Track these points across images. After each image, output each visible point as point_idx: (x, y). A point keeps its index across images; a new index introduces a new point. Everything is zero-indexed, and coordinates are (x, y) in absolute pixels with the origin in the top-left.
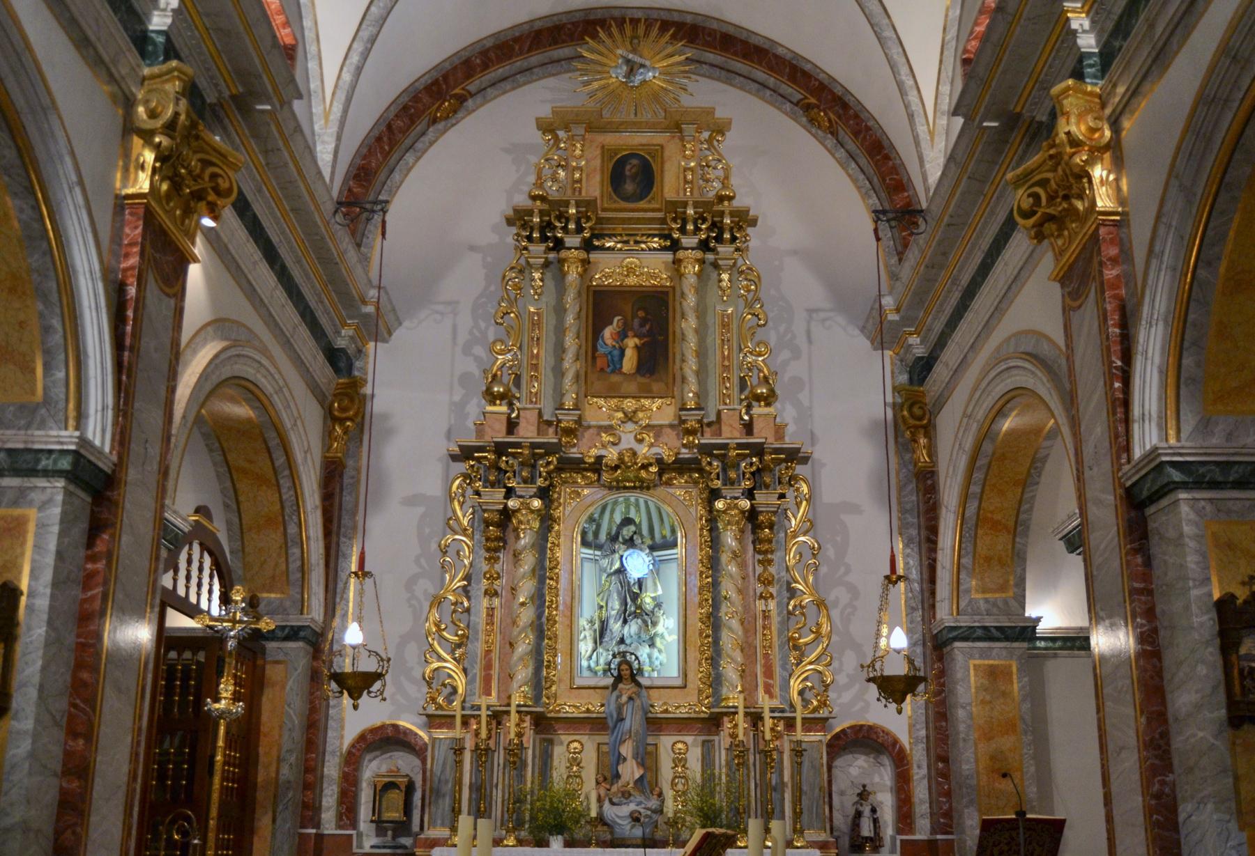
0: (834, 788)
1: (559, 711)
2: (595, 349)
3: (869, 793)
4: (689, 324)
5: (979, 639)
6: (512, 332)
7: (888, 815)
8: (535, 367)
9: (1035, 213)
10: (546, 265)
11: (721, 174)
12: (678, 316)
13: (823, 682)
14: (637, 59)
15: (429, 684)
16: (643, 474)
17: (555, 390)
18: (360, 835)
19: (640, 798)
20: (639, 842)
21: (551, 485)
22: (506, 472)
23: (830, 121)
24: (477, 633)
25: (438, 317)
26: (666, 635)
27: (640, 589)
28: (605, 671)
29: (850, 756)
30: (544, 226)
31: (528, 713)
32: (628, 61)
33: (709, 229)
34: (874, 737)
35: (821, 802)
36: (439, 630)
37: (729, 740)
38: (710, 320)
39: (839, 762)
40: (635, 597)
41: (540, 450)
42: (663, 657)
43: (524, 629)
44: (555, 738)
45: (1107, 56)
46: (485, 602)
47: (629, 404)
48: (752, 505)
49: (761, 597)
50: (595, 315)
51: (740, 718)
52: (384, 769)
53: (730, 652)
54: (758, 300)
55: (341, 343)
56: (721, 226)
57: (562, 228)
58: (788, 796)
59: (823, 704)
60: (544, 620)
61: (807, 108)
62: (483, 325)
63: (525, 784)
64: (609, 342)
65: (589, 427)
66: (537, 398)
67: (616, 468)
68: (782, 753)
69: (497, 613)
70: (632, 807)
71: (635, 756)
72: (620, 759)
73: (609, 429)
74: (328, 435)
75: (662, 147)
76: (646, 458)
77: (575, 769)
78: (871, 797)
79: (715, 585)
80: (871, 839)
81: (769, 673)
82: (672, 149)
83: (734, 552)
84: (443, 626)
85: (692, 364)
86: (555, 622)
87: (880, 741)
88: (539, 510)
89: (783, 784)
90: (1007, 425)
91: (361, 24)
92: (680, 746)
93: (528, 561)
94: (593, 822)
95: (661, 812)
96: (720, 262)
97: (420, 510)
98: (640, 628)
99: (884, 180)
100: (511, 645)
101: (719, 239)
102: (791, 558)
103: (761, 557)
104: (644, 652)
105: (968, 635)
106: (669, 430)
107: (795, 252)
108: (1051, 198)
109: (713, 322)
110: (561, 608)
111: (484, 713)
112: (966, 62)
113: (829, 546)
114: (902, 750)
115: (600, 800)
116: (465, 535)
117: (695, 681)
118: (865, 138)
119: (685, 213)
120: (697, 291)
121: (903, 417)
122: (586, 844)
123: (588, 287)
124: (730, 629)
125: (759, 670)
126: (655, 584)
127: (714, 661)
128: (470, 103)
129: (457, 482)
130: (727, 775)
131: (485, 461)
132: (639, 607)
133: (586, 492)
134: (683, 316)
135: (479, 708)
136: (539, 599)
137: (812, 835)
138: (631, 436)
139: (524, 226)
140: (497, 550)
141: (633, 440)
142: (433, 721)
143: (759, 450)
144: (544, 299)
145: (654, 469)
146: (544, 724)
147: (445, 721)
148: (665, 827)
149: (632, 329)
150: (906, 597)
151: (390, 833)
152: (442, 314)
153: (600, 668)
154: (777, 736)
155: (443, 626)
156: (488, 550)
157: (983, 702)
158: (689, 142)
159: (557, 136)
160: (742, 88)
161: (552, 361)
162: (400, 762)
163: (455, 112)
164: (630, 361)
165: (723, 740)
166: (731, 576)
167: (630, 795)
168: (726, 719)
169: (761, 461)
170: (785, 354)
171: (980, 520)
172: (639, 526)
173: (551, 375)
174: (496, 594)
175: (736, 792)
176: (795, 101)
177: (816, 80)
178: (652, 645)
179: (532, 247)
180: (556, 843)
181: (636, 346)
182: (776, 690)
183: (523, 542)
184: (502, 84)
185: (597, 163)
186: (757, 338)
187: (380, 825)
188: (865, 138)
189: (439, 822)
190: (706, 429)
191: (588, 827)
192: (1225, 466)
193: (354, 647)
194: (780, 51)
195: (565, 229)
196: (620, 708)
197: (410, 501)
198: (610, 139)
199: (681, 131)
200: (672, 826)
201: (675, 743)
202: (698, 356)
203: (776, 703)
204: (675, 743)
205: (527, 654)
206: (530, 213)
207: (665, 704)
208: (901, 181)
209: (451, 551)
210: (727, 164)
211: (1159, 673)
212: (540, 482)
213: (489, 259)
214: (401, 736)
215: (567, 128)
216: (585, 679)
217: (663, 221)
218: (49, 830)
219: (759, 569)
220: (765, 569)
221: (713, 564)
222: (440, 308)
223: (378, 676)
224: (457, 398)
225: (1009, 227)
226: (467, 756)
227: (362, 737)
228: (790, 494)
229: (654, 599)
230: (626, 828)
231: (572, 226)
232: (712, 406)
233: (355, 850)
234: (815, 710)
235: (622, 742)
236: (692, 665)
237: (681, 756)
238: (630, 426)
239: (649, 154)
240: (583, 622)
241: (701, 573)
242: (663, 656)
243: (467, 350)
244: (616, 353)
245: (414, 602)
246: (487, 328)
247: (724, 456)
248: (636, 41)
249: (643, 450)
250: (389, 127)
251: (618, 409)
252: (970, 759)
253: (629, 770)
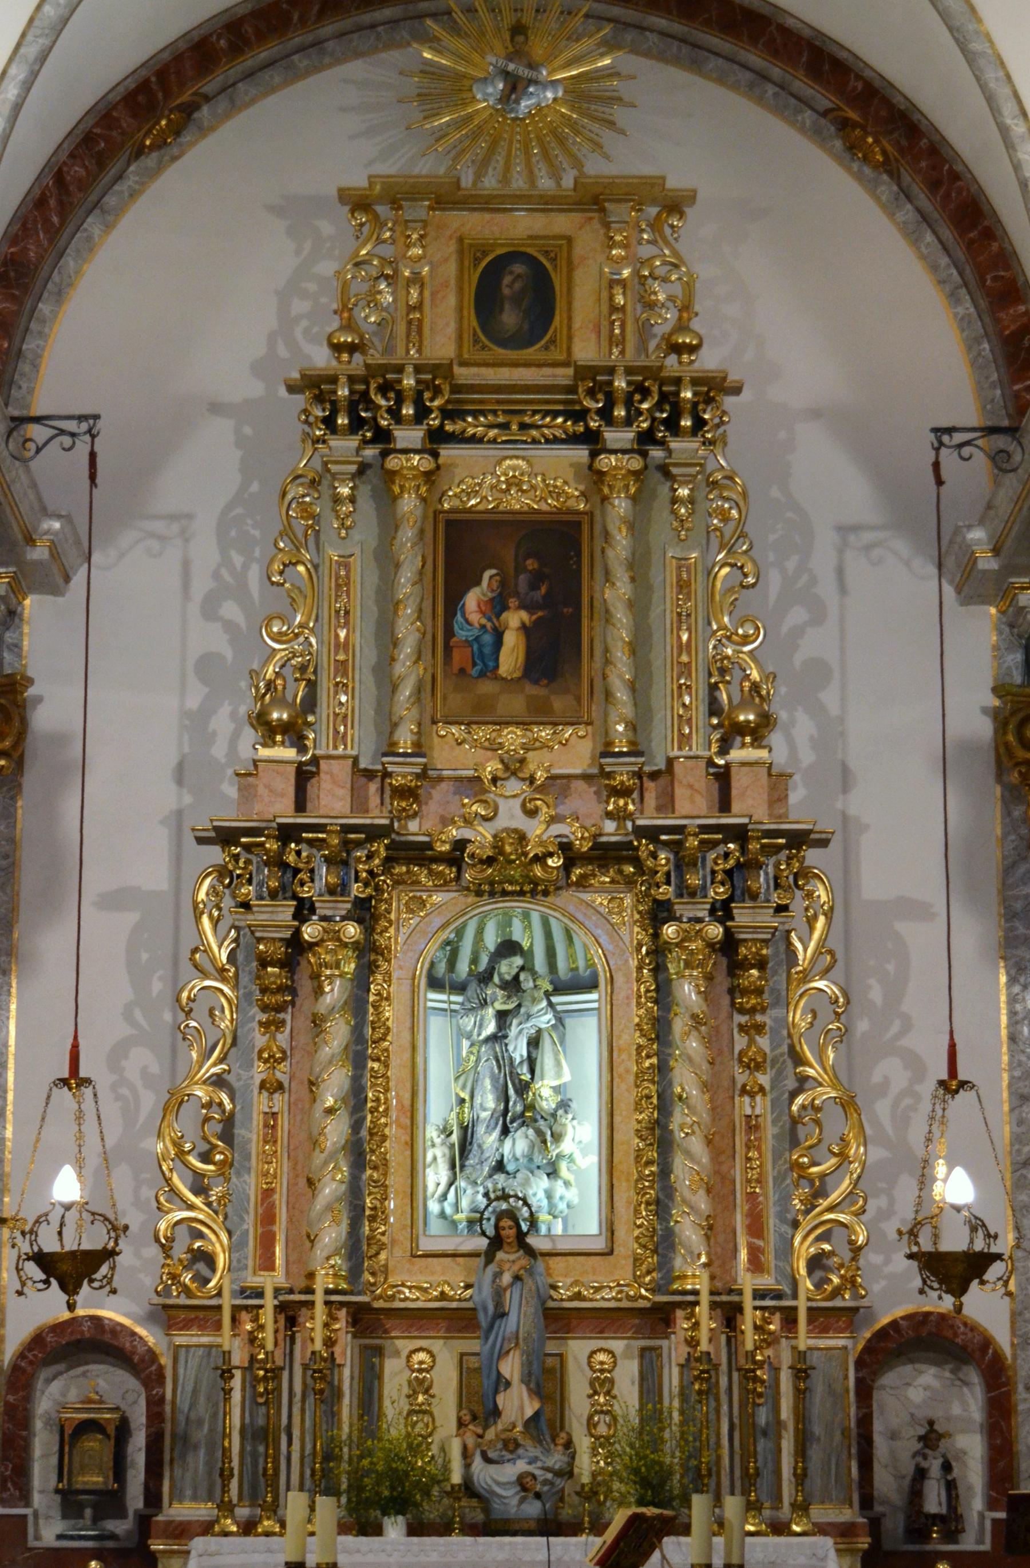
1: (393, 1298)
2: (449, 632)
3: (940, 1436)
4: (616, 594)
6: (300, 600)
7: (974, 1474)
8: (342, 667)
11: (677, 290)
12: (599, 575)
13: (851, 1242)
14: (524, 72)
15: (166, 1250)
16: (538, 871)
17: (378, 711)
18: (36, 1514)
19: (534, 1451)
20: (533, 1525)
21: (378, 889)
22: (297, 871)
23: (884, 152)
24: (247, 1157)
25: (155, 545)
26: (577, 1156)
27: (532, 1071)
28: (471, 1222)
29: (909, 1368)
30: (357, 403)
31: (342, 1304)
32: (506, 74)
33: (659, 406)
34: (949, 1334)
35: (844, 1456)
36: (181, 1154)
37: (685, 1350)
38: (656, 577)
39: (889, 1379)
40: (523, 1088)
41: (355, 836)
42: (572, 1195)
43: (332, 1157)
44: (387, 1343)
46: (261, 1103)
47: (512, 737)
48: (727, 931)
49: (744, 1091)
51: (702, 1310)
52: (73, 1396)
53: (687, 1194)
54: (743, 535)
56: (670, 406)
57: (389, 410)
58: (787, 1445)
59: (850, 1282)
60: (364, 1133)
61: (844, 125)
62: (238, 560)
63: (340, 1428)
64: (475, 618)
65: (440, 779)
67: (490, 861)
68: (776, 1370)
69: (284, 1123)
71: (527, 1379)
72: (501, 1383)
75: (569, 240)
76: (542, 843)
77: (421, 1398)
78: (943, 1444)
79: (663, 1069)
82: (587, 240)
83: (694, 1017)
84: (188, 1146)
86: (384, 1138)
87: (958, 1340)
88: (357, 942)
89: (779, 1424)
91: (23, 35)
92: (602, 1357)
93: (338, 1033)
94: (453, 1493)
95: (570, 1474)
96: (675, 471)
97: (132, 918)
98: (532, 1146)
99: (983, 281)
100: (310, 1182)
102: (799, 1018)
103: (743, 1019)
104: (538, 1189)
106: (580, 785)
107: (816, 414)
110: (394, 1114)
111: (269, 1302)
113: (872, 981)
114: (998, 1358)
116: (224, 980)
118: (948, 195)
119: (611, 383)
120: (631, 527)
121: (1007, 745)
122: (444, 1529)
123: (436, 513)
124: (688, 1154)
125: (740, 1221)
126: (558, 1064)
127: (661, 1206)
128: (205, 112)
129: (208, 882)
130: (682, 1412)
131: (261, 854)
132: (531, 1107)
133: (437, 898)
135: (260, 1294)
136: (356, 1099)
140: (280, 1008)
141: (518, 811)
143: (740, 834)
144: (356, 536)
146: (369, 1321)
148: (576, 1499)
149: (516, 594)
150: (1012, 1078)
151: (88, 1512)
152: (162, 538)
153: (461, 1216)
154: (770, 1341)
155: (188, 1146)
156: (265, 1008)
158: (620, 231)
159: (376, 217)
160: (721, 80)
162: (102, 1383)
163: (178, 133)
165: (674, 1350)
166: (690, 1060)
167: (517, 1445)
168: (680, 1313)
169: (743, 850)
172: (528, 955)
173: (370, 681)
174: (280, 1087)
175: (696, 1440)
176: (821, 109)
177: (859, 77)
178: (553, 1173)
179: (335, 442)
180: (394, 1528)
181: (523, 627)
182: (770, 1258)
183: (328, 999)
184: (266, 75)
186: (738, 613)
187: (70, 1501)
188: (948, 195)
189: (189, 1493)
190: (649, 785)
191: (446, 1501)
193: (68, 1207)
194: (790, 22)
195: (395, 413)
196: (499, 1294)
197: (115, 900)
198: (475, 224)
199: (603, 210)
200: (588, 1499)
201: (594, 1352)
202: (633, 652)
203: (767, 1281)
204: (594, 1352)
205: (339, 1199)
206: (334, 380)
207: (576, 1283)
208: (1013, 281)
209: (200, 1009)
210: (689, 273)
212: (356, 889)
213: (248, 430)
214: (107, 1337)
216: (435, 1236)
217: (572, 390)
219: (740, 1042)
220: (752, 1042)
221: (659, 1030)
223: (108, 1254)
224: (193, 703)
226: (236, 1383)
227: (37, 1340)
228: (798, 904)
229: (557, 1090)
230: (510, 1502)
232: (662, 747)
233: (32, 1543)
234: (837, 1292)
235: (503, 1354)
236: (624, 1212)
237: (604, 1372)
238: (513, 786)
239: (546, 253)
240: (432, 1133)
241: (639, 1048)
242: (572, 1197)
243: (210, 610)
244: (487, 638)
245: (124, 1091)
246: (246, 567)
247: (679, 844)
248: (520, 39)
249: (536, 829)
250: (59, 178)
253: (516, 1403)
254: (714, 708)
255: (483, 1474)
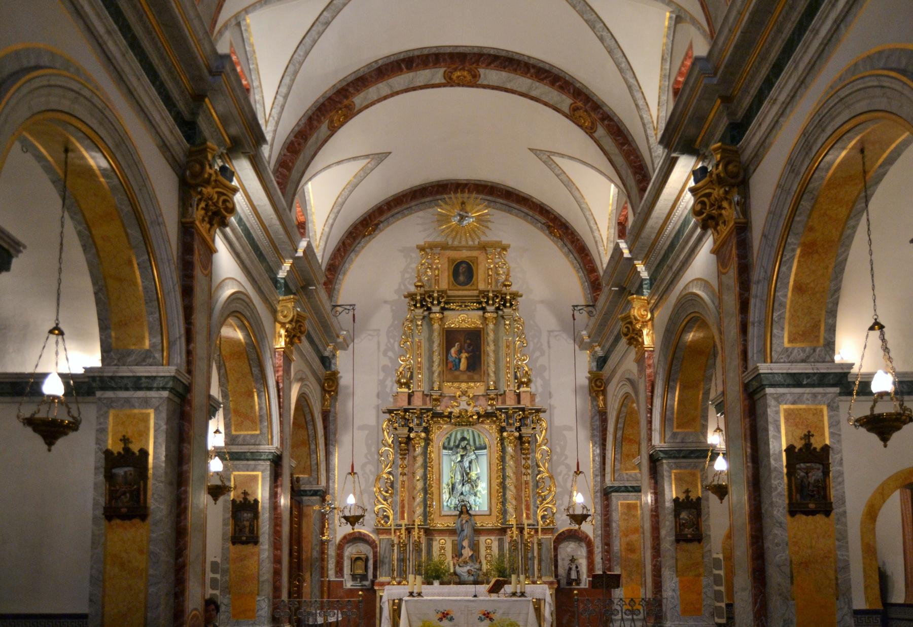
0: (559, 557)
2: (447, 359)
4: (491, 348)
5: (623, 492)
7: (584, 569)
9: (703, 213)
10: (424, 317)
11: (505, 270)
15: (377, 515)
32: (460, 215)
40: (467, 474)
41: (423, 411)
42: (480, 500)
45: (653, 279)
46: (401, 478)
47: (464, 386)
50: (447, 342)
51: (514, 529)
52: (354, 551)
55: (326, 354)
58: (536, 562)
59: (552, 522)
61: (549, 227)
62: (392, 341)
64: (454, 355)
66: (420, 384)
67: (458, 417)
69: (406, 483)
70: (468, 568)
71: (469, 546)
72: (463, 547)
73: (454, 398)
74: (323, 398)
79: (504, 469)
80: (575, 580)
81: (528, 508)
85: (492, 368)
90: (690, 337)
93: (420, 460)
101: (504, 305)
104: (472, 499)
105: (618, 490)
107: (542, 302)
108: (712, 205)
109: (502, 344)
111: (404, 528)
112: (676, 92)
114: (590, 540)
115: (454, 565)
117: (495, 513)
125: (524, 507)
127: (504, 503)
134: (488, 344)
136: (425, 477)
137: (544, 579)
138: (465, 403)
139: (412, 299)
140: (405, 454)
142: (378, 531)
143: (523, 410)
145: (475, 417)
146: (429, 533)
147: (387, 531)
154: (532, 536)
157: (624, 520)
161: (427, 365)
164: (463, 365)
165: (507, 539)
170: (537, 354)
171: (623, 438)
172: (468, 441)
174: (405, 474)
178: (476, 495)
179: (417, 311)
182: (531, 516)
185: (446, 265)
187: (354, 577)
192: (679, 451)
196: (462, 525)
197: (362, 428)
203: (531, 522)
209: (385, 455)
211: (658, 522)
215: (431, 249)
216: (446, 511)
217: (478, 296)
218: (271, 580)
219: (523, 462)
221: (503, 459)
222: (371, 333)
223: (362, 516)
224: (381, 377)
225: (617, 340)
226: (396, 548)
227: (345, 537)
228: (538, 427)
230: (465, 577)
231: (435, 302)
234: (549, 524)
235: (463, 540)
237: (490, 546)
238: (464, 398)
240: (444, 485)
242: (481, 500)
243: (385, 354)
249: (470, 409)
250: (344, 243)
251: (459, 388)
252: (617, 545)
254: (516, 378)
255: (458, 570)
